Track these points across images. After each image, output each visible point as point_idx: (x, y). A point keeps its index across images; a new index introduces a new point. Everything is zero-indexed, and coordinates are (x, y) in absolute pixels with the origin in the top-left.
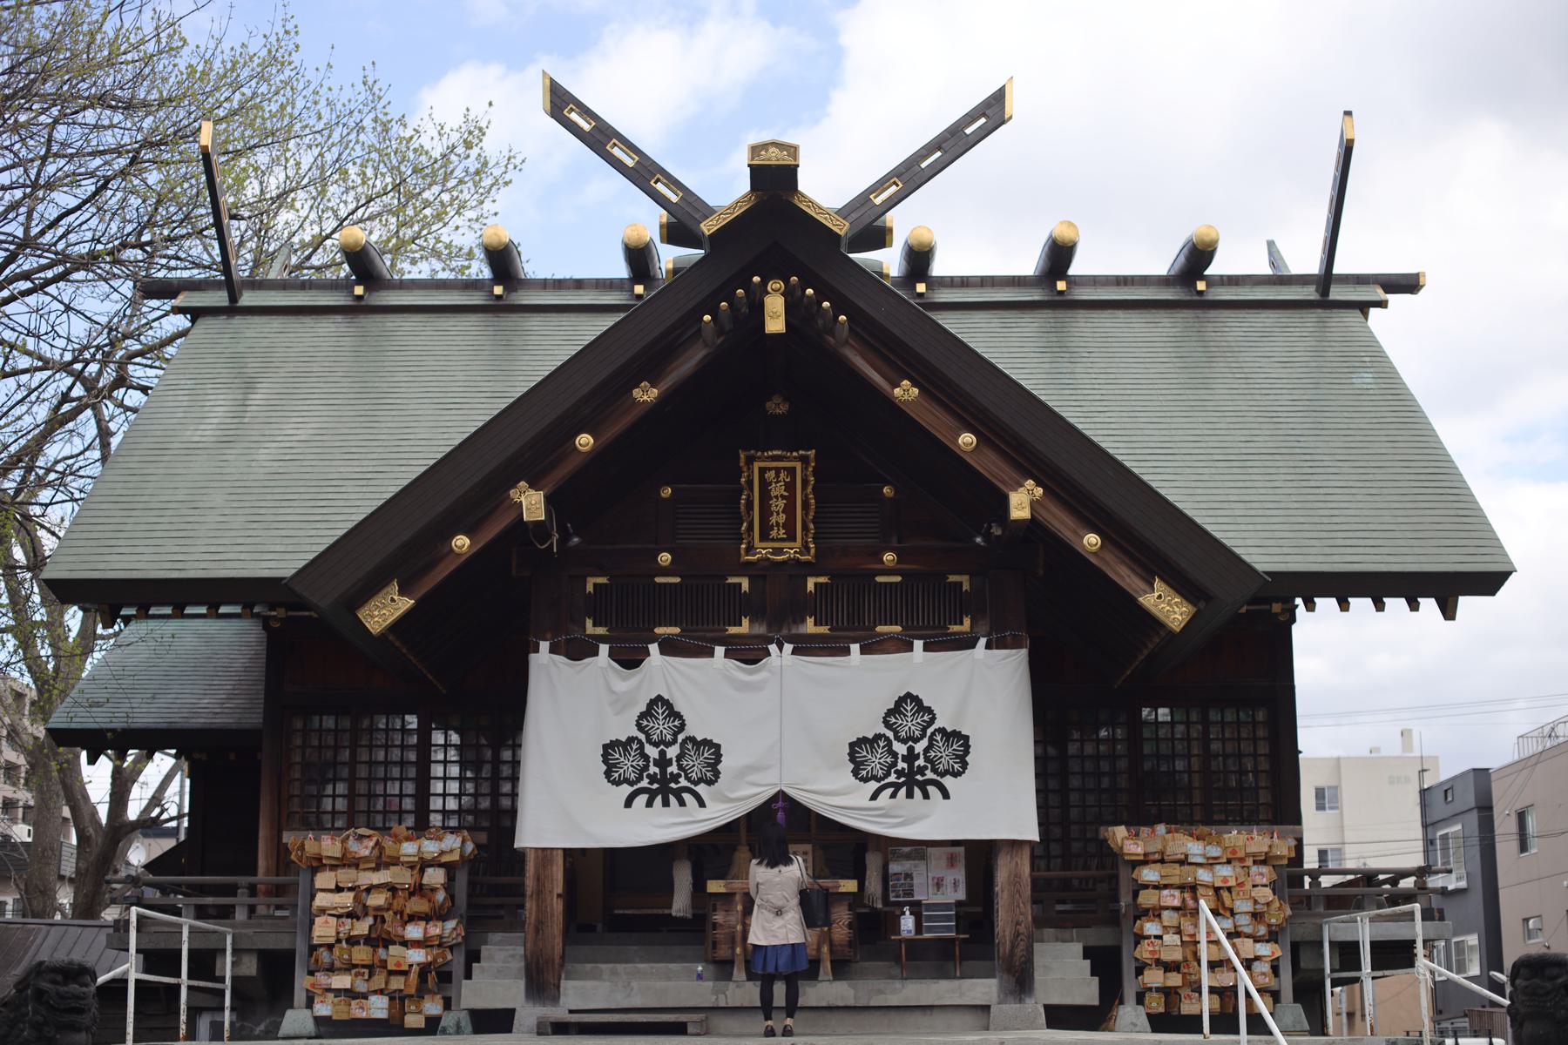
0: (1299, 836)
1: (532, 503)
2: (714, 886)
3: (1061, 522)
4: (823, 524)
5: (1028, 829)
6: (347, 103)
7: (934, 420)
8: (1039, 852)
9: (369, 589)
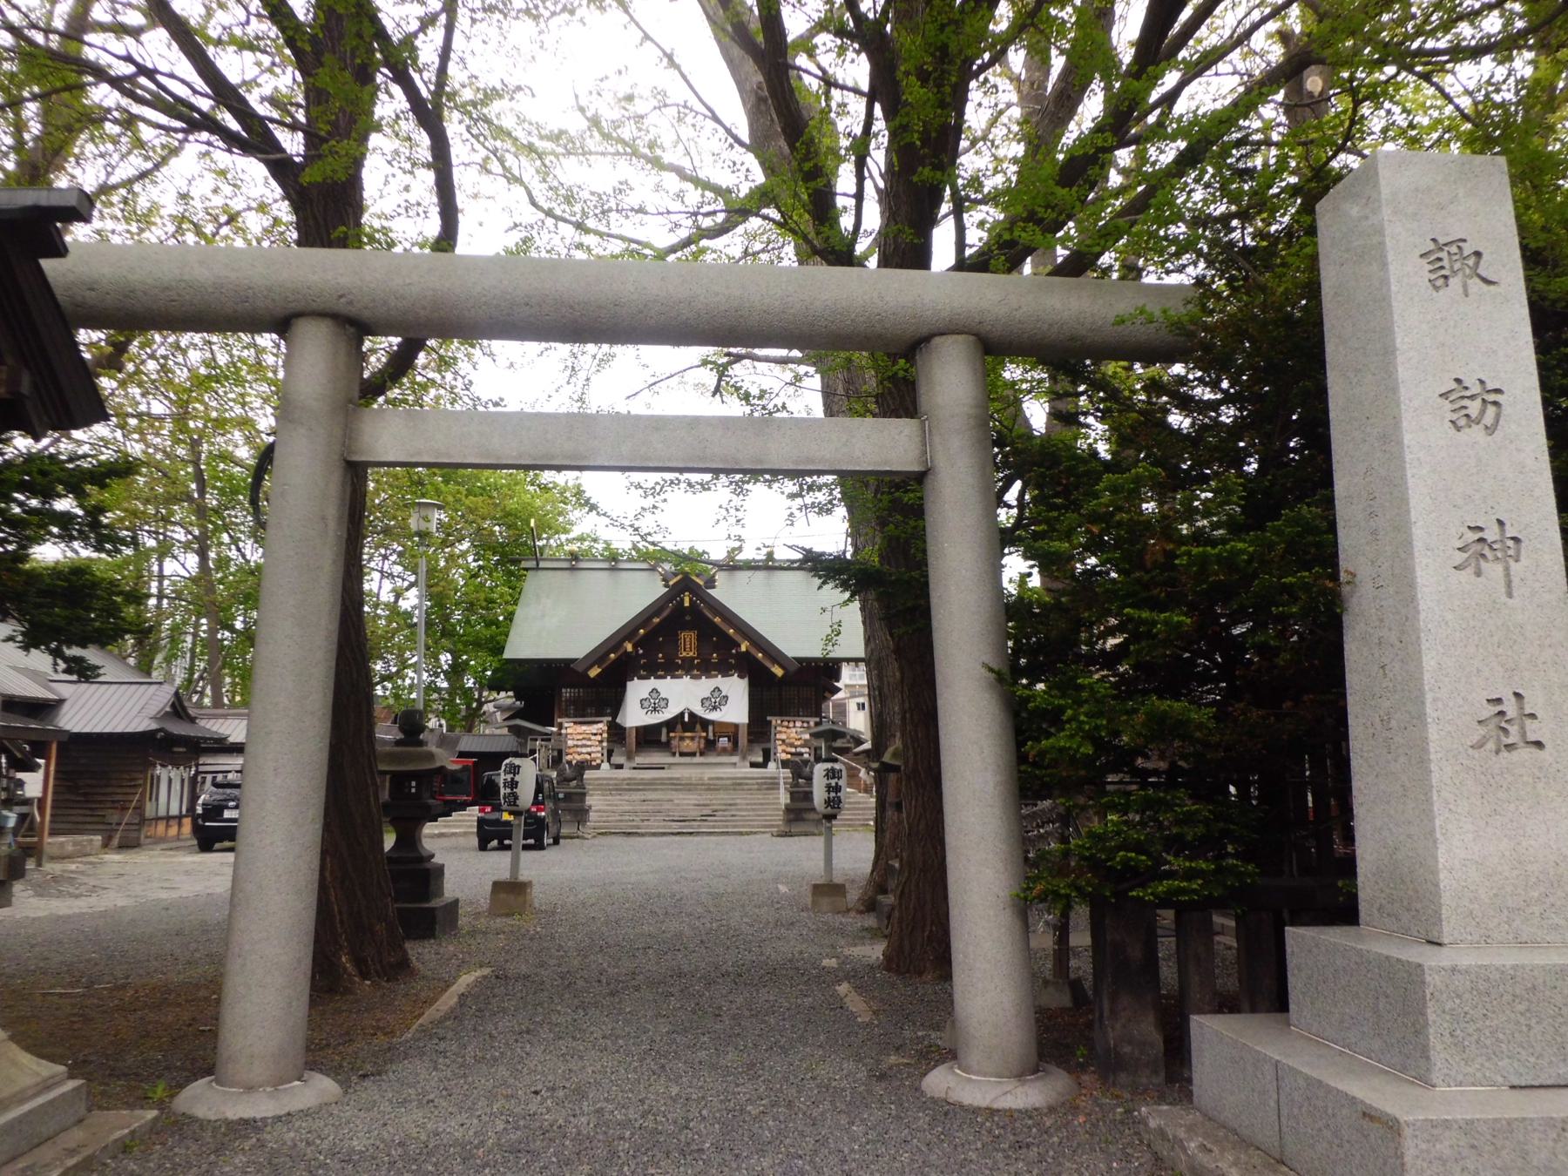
0: (349, 242)
1: (629, 647)
2: (672, 735)
3: (753, 651)
4: (698, 648)
5: (746, 720)
6: (740, 515)
7: (724, 626)
8: (749, 725)
9: (591, 667)
